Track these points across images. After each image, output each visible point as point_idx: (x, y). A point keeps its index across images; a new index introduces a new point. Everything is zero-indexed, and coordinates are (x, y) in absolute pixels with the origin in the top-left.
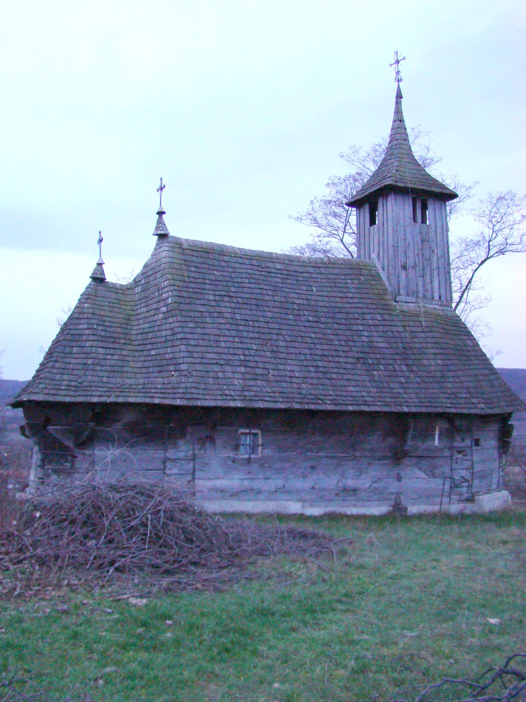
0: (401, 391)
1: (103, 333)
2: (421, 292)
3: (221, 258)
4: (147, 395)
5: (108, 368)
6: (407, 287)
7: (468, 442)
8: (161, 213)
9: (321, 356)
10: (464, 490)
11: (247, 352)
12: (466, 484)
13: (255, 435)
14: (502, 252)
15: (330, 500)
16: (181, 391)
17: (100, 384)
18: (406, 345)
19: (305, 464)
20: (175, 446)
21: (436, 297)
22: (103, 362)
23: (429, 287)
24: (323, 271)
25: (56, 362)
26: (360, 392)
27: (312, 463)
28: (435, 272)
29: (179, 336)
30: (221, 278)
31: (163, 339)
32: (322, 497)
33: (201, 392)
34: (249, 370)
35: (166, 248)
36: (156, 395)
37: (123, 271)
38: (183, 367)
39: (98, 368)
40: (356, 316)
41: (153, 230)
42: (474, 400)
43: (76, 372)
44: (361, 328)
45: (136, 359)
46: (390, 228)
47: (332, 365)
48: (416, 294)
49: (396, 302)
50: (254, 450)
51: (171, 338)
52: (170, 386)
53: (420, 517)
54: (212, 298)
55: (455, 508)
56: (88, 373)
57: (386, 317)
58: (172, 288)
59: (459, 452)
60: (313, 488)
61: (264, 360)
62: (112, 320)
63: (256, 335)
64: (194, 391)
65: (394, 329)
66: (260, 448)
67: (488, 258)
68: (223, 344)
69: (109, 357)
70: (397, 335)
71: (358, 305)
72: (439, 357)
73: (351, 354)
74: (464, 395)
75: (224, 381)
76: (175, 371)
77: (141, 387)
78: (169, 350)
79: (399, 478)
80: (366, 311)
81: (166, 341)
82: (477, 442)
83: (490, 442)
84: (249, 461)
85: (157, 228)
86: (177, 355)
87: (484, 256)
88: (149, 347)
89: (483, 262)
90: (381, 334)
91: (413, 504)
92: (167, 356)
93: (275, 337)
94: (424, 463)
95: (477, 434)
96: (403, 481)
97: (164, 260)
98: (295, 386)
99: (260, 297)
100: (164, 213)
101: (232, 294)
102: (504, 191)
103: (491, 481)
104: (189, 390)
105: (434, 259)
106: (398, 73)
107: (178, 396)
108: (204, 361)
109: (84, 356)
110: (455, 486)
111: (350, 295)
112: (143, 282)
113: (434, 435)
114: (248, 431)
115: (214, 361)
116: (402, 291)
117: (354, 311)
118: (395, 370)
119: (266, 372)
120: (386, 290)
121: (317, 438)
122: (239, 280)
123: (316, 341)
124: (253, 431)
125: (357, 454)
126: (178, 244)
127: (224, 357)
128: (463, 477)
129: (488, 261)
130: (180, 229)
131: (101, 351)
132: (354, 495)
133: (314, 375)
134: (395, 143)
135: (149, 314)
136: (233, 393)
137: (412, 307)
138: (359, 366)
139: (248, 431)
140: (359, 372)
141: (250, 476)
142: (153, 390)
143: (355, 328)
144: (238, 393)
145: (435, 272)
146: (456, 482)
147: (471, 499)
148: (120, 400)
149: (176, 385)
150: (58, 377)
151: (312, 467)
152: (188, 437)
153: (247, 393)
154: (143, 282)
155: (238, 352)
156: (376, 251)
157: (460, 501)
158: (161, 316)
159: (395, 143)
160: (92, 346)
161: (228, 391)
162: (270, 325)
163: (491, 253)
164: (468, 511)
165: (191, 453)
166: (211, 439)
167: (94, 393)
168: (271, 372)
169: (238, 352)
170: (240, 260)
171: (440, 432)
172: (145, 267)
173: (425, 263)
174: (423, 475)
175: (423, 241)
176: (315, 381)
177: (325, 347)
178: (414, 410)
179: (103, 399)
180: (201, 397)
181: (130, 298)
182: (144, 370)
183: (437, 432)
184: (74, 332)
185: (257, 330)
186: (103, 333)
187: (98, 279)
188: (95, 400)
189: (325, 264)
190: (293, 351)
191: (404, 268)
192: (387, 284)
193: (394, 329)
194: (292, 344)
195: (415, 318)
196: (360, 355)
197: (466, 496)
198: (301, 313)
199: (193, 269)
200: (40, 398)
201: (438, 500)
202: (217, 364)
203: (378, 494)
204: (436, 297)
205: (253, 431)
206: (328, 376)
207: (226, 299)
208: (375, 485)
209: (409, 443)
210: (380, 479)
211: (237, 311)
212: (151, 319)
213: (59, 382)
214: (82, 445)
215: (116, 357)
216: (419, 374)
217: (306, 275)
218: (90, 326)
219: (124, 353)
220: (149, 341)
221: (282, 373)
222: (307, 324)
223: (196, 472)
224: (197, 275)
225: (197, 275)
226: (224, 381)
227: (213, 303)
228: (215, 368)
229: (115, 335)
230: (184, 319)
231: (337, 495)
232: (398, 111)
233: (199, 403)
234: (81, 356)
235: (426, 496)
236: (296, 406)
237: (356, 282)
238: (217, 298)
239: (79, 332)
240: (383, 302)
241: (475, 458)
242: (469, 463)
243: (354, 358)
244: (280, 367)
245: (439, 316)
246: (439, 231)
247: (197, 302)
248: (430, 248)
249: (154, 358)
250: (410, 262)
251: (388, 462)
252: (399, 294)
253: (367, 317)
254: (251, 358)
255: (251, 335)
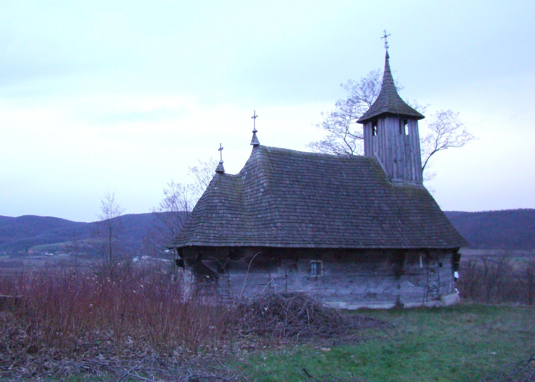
0: (400, 236)
1: (228, 205)
2: (405, 175)
3: (289, 157)
4: (261, 241)
5: (235, 226)
6: (397, 172)
7: (436, 265)
8: (255, 132)
9: (353, 216)
10: (435, 293)
11: (312, 215)
12: (435, 290)
13: (320, 263)
14: (445, 147)
15: (361, 301)
16: (280, 239)
17: (232, 236)
18: (399, 208)
19: (347, 280)
20: (276, 271)
21: (414, 178)
22: (231, 222)
23: (410, 173)
24: (347, 164)
25: (204, 222)
26: (377, 237)
27: (351, 279)
28: (413, 164)
29: (273, 206)
30: (292, 170)
31: (264, 208)
32: (357, 299)
33: (291, 239)
34: (315, 225)
35: (259, 153)
36: (267, 242)
37: (233, 168)
38: (279, 225)
39: (230, 226)
40: (370, 191)
41: (250, 141)
42: (441, 241)
43: (217, 229)
44: (373, 198)
45: (249, 220)
46: (387, 138)
47: (360, 221)
48: (402, 177)
49: (391, 182)
50: (318, 272)
51: (269, 207)
52: (273, 236)
53: (412, 309)
54: (288, 182)
55: (431, 304)
56: (224, 229)
57: (387, 191)
58: (266, 177)
59: (432, 271)
60: (352, 294)
61: (322, 219)
62: (232, 197)
63: (316, 204)
64: (287, 239)
65: (392, 199)
66: (322, 271)
67: (435, 151)
68: (298, 210)
69: (234, 219)
70: (394, 202)
71: (370, 185)
72: (419, 215)
73: (369, 215)
74: (435, 238)
75: (302, 233)
76: (274, 227)
77: (256, 237)
78: (269, 215)
79: (399, 287)
80: (375, 188)
81: (266, 209)
82: (441, 265)
83: (447, 265)
84: (316, 278)
85: (253, 141)
86: (274, 218)
87: (434, 149)
88: (256, 213)
89: (433, 153)
90: (385, 202)
91: (407, 302)
92: (268, 218)
93: (326, 205)
94: (413, 278)
95: (441, 260)
96: (401, 288)
97: (259, 160)
98: (341, 234)
99: (314, 181)
100: (256, 131)
101: (299, 180)
102: (445, 110)
103: (449, 287)
104: (284, 238)
105: (410, 156)
106: (386, 43)
107: (279, 242)
108: (290, 221)
109: (220, 219)
110: (430, 290)
111: (364, 178)
112: (246, 173)
113: (419, 261)
114: (315, 261)
115: (295, 221)
116: (395, 175)
117: (369, 188)
118: (395, 224)
119: (324, 226)
120: (384, 175)
121: (353, 264)
122: (302, 171)
123: (349, 207)
124: (318, 261)
125: (376, 273)
126: (265, 150)
127: (300, 218)
128: (434, 286)
129: (436, 152)
130: (265, 141)
131: (229, 215)
132: (374, 297)
133: (350, 227)
134: (386, 85)
135: (253, 193)
136: (308, 239)
137: (400, 184)
138: (375, 221)
139: (315, 261)
140: (375, 225)
141: (316, 287)
142: (264, 239)
143: (370, 198)
144: (311, 239)
145: (413, 164)
146: (431, 289)
147: (439, 299)
148: (247, 245)
149: (276, 236)
150: (207, 232)
151: (351, 282)
152: (282, 265)
153: (316, 239)
154: (246, 173)
155: (307, 215)
156: (377, 151)
157: (433, 300)
158: (261, 194)
159: (386, 85)
160: (223, 213)
161: (304, 238)
162: (323, 198)
163: (438, 147)
164: (438, 306)
165: (284, 274)
166: (295, 267)
167: (230, 241)
168: (327, 226)
169: (307, 215)
170: (301, 159)
171: (422, 260)
172: (246, 164)
173: (407, 158)
174: (412, 285)
175: (405, 145)
176: (352, 231)
177: (355, 211)
178: (409, 247)
179: (237, 244)
180: (291, 242)
181: (240, 183)
182: (256, 227)
183: (421, 260)
184: (212, 204)
185: (315, 201)
186: (228, 205)
187: (220, 172)
188: (232, 245)
189: (348, 159)
190: (337, 213)
191: (395, 161)
192: (385, 171)
193: (392, 199)
194: (337, 209)
195: (403, 192)
196: (375, 215)
197: (436, 296)
198: (339, 190)
199: (276, 165)
200: (199, 244)
201: (422, 299)
202: (296, 222)
203: (388, 297)
204: (414, 178)
205: (318, 261)
206: (359, 228)
207: (296, 183)
208: (386, 291)
209: (406, 266)
210: (388, 288)
211: (303, 190)
212: (255, 196)
213: (208, 235)
214: (221, 271)
215: (238, 219)
216: (409, 225)
217: (338, 167)
218: (221, 201)
219: (242, 216)
220: (256, 209)
221: (333, 227)
222: (343, 197)
223: (288, 286)
224: (278, 169)
225: (278, 169)
226: (302, 233)
227: (289, 186)
228: (296, 225)
229: (236, 206)
230: (275, 196)
231: (365, 297)
232: (387, 66)
233: (291, 246)
234: (218, 219)
235: (412, 297)
236: (344, 246)
237: (367, 170)
238: (291, 182)
239: (214, 204)
240: (383, 182)
241: (440, 274)
242: (437, 277)
243: (371, 216)
244: (332, 223)
245: (416, 189)
246: (414, 138)
247: (280, 185)
248: (410, 149)
249: (261, 219)
250: (399, 157)
251: (392, 277)
252: (393, 177)
253: (376, 191)
254: (315, 219)
255: (313, 205)
